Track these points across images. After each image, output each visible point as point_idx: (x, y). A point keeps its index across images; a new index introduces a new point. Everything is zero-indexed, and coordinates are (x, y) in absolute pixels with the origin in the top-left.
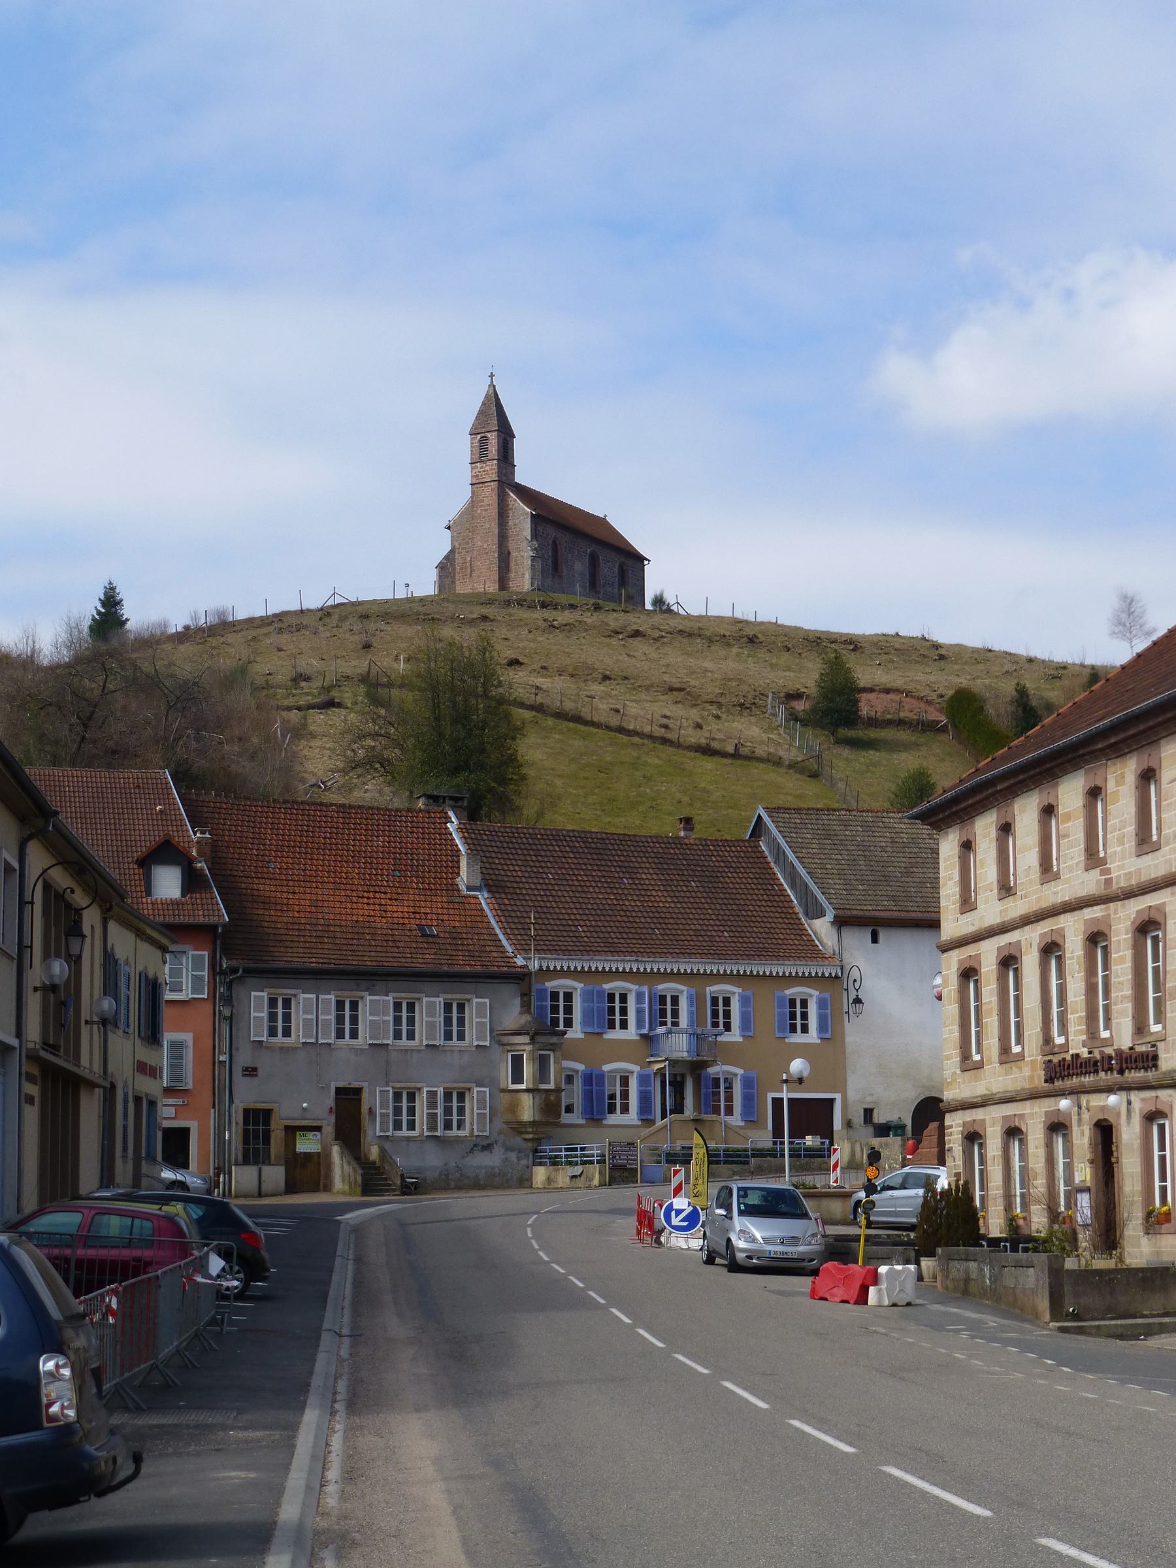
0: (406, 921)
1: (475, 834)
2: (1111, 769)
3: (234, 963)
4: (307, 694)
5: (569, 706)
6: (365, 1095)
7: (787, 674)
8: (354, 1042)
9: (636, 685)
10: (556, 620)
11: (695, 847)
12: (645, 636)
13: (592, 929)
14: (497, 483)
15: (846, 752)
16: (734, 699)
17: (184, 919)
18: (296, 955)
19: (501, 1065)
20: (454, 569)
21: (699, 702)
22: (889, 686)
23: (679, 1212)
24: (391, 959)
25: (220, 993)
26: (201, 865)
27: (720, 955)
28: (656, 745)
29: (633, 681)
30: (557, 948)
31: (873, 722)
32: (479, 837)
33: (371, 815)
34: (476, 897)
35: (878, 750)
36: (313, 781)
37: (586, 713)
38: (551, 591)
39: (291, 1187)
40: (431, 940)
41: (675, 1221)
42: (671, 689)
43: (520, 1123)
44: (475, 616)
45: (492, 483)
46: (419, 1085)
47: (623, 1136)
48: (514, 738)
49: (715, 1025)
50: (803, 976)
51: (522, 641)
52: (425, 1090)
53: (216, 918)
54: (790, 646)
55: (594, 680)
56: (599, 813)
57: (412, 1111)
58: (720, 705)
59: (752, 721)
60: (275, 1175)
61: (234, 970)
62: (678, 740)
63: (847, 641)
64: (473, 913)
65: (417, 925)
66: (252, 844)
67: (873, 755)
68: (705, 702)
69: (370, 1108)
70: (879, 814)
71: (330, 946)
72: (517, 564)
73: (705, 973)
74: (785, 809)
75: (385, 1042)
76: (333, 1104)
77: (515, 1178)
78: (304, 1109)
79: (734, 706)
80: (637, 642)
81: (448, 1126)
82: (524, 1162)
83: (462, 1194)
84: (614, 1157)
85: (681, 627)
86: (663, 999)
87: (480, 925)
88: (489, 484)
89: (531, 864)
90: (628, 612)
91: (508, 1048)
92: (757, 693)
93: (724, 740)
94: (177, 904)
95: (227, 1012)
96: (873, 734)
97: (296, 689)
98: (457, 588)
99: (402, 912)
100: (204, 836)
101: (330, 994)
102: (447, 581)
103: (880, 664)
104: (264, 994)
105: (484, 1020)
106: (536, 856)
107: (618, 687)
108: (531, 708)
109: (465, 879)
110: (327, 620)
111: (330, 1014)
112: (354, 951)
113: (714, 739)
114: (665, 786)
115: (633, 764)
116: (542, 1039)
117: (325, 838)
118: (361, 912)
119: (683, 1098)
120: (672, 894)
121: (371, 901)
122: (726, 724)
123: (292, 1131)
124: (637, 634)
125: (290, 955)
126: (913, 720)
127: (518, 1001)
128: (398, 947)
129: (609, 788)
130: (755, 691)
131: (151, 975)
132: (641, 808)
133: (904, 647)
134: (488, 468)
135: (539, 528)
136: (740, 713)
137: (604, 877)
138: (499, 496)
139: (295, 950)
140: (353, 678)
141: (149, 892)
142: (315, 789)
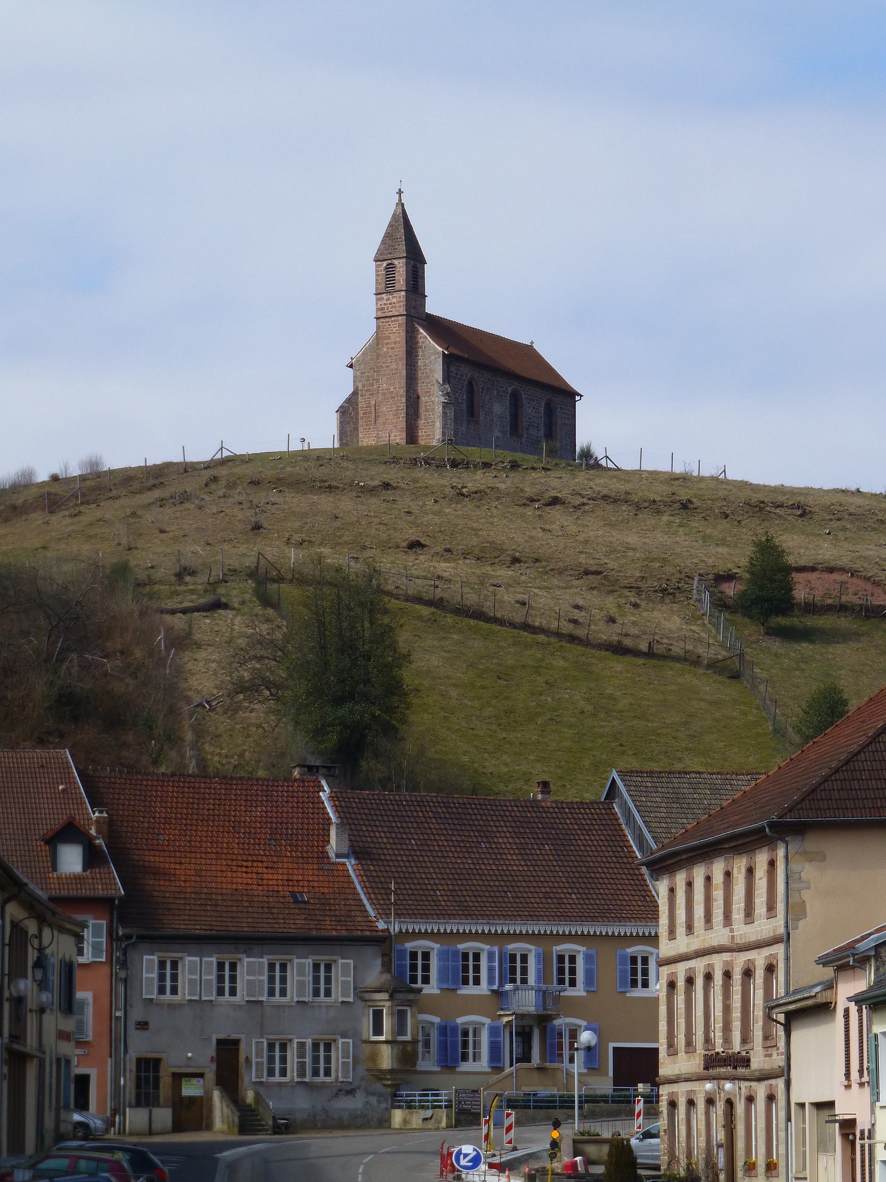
0: (281, 889)
1: (345, 802)
2: (736, 861)
3: (128, 931)
4: (192, 592)
5: (471, 599)
6: (243, 1046)
7: (720, 550)
8: (232, 999)
9: (548, 568)
10: (466, 487)
11: (552, 810)
12: (564, 503)
13: (449, 893)
14: (405, 317)
15: (776, 645)
16: (656, 584)
17: (85, 892)
18: (182, 922)
19: (364, 1019)
20: (357, 413)
21: (616, 588)
22: (833, 564)
23: (466, 1155)
24: (266, 925)
25: (117, 957)
26: (99, 842)
27: (567, 917)
28: (563, 644)
29: (544, 564)
30: (416, 912)
31: (811, 608)
32: (349, 805)
33: (251, 785)
34: (344, 864)
35: (812, 642)
36: (197, 700)
37: (488, 608)
38: (462, 444)
39: (178, 1127)
40: (302, 906)
41: (463, 1162)
42: (587, 573)
43: (381, 1071)
44: (376, 483)
45: (400, 318)
46: (290, 1037)
47: (469, 1083)
48: (400, 667)
49: (561, 981)
50: (644, 936)
51: (427, 514)
52: (296, 1041)
53: (113, 892)
54: (728, 512)
55: (502, 563)
56: (494, 727)
57: (283, 1060)
58: (639, 591)
59: (675, 609)
60: (164, 1116)
61: (128, 937)
62: (587, 637)
63: (794, 504)
64: (342, 879)
65: (290, 892)
66: (144, 817)
67: (806, 648)
68: (622, 588)
69: (247, 1057)
70: (728, 776)
71: (213, 914)
72: (427, 411)
73: (552, 934)
74: (638, 772)
75: (261, 999)
76: (214, 1054)
77: (375, 1119)
78: (189, 1058)
79: (656, 591)
80: (555, 512)
81: (316, 1073)
82: (383, 1105)
83: (327, 1134)
84: (460, 1102)
85: (605, 492)
86: (513, 958)
87: (347, 891)
88: (396, 318)
89: (396, 830)
90: (549, 469)
91: (370, 1004)
92: (682, 576)
93: (638, 637)
94: (75, 879)
95: (122, 975)
96: (811, 621)
97: (180, 585)
98: (360, 435)
99: (277, 880)
100: (101, 815)
101: (212, 957)
102: (349, 428)
103: (829, 534)
104: (155, 958)
105: (349, 979)
106: (400, 822)
107: (528, 571)
108: (430, 603)
109: (334, 847)
110: (213, 486)
111: (212, 975)
112: (233, 918)
113: (627, 635)
114: (567, 693)
115: (536, 667)
116: (400, 996)
117: (208, 810)
118: (240, 881)
119: (530, 1048)
120: (526, 857)
121: (249, 870)
122: (645, 614)
123: (178, 1078)
124: (555, 501)
125: (177, 922)
126: (856, 605)
127: (379, 962)
128: (272, 914)
129: (507, 698)
130: (680, 572)
131: (67, 958)
132: (540, 721)
133: (860, 511)
134: (394, 300)
135: (452, 369)
136: (662, 601)
137: (463, 841)
138: (407, 332)
139: (182, 917)
140: (240, 572)
141: (54, 868)
142: (199, 709)
